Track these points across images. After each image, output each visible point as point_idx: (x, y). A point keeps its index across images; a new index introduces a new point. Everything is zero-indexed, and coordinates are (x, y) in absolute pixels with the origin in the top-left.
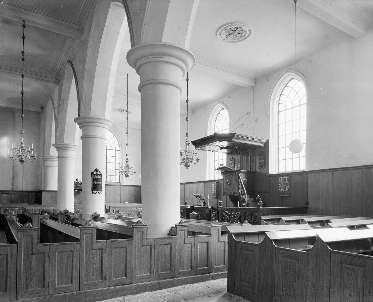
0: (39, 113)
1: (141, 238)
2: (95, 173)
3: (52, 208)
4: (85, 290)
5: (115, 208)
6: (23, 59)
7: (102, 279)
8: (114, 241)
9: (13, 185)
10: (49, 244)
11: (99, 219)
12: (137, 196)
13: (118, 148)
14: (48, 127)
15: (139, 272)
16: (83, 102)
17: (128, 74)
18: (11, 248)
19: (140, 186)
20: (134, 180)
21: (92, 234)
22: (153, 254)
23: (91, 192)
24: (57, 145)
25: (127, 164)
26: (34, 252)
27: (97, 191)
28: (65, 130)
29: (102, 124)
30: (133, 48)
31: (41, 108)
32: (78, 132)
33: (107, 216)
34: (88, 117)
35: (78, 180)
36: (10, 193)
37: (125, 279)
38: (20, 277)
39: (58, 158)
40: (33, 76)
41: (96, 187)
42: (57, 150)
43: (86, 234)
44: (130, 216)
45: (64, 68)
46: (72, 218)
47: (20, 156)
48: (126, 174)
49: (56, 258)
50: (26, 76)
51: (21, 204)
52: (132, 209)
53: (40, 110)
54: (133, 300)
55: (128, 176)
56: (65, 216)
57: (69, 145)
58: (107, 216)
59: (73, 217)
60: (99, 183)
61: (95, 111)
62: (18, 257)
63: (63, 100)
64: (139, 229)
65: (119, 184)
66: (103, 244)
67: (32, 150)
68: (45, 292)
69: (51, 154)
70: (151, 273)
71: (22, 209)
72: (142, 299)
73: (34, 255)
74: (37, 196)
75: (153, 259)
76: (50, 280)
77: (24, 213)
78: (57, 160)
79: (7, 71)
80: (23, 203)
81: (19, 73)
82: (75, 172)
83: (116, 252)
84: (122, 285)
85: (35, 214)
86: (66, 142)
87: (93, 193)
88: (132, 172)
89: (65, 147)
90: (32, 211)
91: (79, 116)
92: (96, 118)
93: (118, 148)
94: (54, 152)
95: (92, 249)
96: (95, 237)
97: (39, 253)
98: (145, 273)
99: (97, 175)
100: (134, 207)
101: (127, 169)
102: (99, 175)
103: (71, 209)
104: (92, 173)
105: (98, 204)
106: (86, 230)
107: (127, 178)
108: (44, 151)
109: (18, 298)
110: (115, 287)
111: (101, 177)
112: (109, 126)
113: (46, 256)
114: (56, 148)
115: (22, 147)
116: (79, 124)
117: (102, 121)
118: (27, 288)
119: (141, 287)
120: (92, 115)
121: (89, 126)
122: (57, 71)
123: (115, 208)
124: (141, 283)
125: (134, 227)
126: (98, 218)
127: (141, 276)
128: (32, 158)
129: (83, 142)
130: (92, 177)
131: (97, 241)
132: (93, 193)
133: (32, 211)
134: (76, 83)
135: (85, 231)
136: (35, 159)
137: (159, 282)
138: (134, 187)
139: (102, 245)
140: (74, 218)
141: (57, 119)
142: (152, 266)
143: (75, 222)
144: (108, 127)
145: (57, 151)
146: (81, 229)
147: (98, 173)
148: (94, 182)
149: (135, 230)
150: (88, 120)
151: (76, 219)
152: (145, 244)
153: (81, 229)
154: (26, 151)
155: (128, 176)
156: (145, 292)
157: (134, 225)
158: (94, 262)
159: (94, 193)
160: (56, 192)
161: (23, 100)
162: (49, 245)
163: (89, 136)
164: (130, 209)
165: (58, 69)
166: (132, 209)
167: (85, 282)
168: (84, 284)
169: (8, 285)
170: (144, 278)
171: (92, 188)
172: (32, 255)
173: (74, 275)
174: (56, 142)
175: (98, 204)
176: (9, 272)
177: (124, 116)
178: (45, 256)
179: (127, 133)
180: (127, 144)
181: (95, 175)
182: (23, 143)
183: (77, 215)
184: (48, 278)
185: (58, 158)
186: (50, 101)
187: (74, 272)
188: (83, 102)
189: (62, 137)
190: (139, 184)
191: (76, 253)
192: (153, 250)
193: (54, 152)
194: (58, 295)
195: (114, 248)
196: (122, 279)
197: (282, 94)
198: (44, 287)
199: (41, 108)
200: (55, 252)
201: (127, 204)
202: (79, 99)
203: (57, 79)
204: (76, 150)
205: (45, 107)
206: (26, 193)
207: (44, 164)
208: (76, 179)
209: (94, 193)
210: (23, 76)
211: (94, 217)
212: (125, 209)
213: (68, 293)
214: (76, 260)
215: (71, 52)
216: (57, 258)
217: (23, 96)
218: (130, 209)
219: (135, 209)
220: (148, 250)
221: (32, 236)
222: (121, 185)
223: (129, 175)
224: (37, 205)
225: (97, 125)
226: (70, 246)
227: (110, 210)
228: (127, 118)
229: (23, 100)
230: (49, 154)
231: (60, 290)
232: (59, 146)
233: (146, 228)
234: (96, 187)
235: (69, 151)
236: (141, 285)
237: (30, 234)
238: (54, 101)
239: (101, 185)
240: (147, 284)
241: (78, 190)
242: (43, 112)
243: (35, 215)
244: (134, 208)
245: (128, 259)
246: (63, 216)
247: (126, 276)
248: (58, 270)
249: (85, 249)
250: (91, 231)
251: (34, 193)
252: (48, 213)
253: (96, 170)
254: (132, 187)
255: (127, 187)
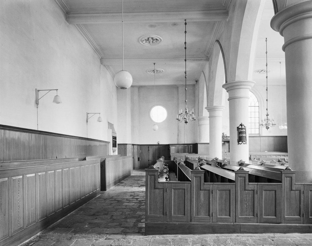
0: (194, 85)
1: (289, 183)
2: (240, 127)
3: (205, 156)
4: (239, 222)
5: (261, 156)
6: (185, 48)
7: (254, 216)
8: (264, 184)
9: (178, 140)
10: (212, 183)
11: (244, 165)
12: (281, 145)
13: (257, 105)
14: (201, 95)
15: (288, 213)
16: (229, 70)
17: (266, 38)
18: (186, 185)
19: (287, 136)
20: (282, 129)
21: (245, 177)
22: (302, 198)
23: (237, 143)
24: (208, 107)
25: (267, 117)
26: (202, 189)
27: (242, 142)
28: (214, 95)
29: (245, 86)
30: (277, 14)
31: (196, 81)
32: (225, 94)
33: (251, 163)
34: (234, 82)
35: (224, 134)
36: (176, 145)
37: (274, 218)
38: (193, 206)
39: (209, 117)
40: (191, 59)
41: (241, 139)
42: (208, 112)
43: (240, 177)
44: (272, 163)
45: (213, 47)
46: (223, 164)
47: (185, 118)
48: (266, 127)
49: (217, 194)
50: (188, 60)
51: (184, 153)
52: (272, 157)
53: (195, 83)
54: (283, 238)
55: (269, 128)
56: (217, 162)
57: (219, 106)
58: (251, 163)
59: (224, 164)
60: (244, 135)
61: (239, 76)
62: (192, 191)
63: (212, 72)
64: (288, 175)
65: (258, 135)
66: (254, 186)
67: (193, 113)
68: (210, 220)
69: (204, 115)
70: (300, 217)
71: (185, 157)
72: (293, 239)
73: (202, 191)
74: (194, 148)
75: (302, 203)
76: (214, 211)
77: (187, 160)
78: (209, 119)
79: (173, 59)
80: (185, 152)
81: (182, 59)
82: (223, 127)
83: (266, 194)
84: (272, 223)
85: (195, 161)
86: (215, 104)
87: (239, 143)
88: (273, 124)
89: (215, 109)
90: (192, 158)
91: (226, 82)
92: (239, 82)
93: (257, 105)
94: (206, 113)
95: (245, 190)
96: (248, 180)
97: (205, 190)
98: (294, 216)
99: (242, 129)
100: (273, 155)
101: (267, 122)
102: (243, 128)
103: (220, 158)
104: (238, 127)
105: (243, 153)
106: (240, 174)
107: (267, 130)
108: (198, 113)
109: (192, 221)
110: (270, 224)
111: (246, 130)
112: (251, 86)
113: (210, 193)
114: (208, 110)
115: (186, 112)
116: (226, 89)
117: (244, 83)
118: (198, 215)
119: (290, 227)
120: (237, 79)
121: (235, 89)
122: (207, 51)
123: (261, 156)
124: (290, 224)
125: (282, 173)
126: (244, 164)
127: (290, 218)
128: (193, 119)
129: (229, 103)
130: (238, 130)
131: (249, 183)
132: (239, 143)
133: (192, 158)
134: (223, 56)
135: (240, 175)
136: (195, 120)
137: (309, 226)
138: (273, 138)
139: (253, 187)
140: (224, 164)
141: (208, 88)
142: (301, 210)
143: (225, 167)
144: (250, 87)
145: (209, 113)
146: (236, 173)
147: (243, 127)
148: (239, 134)
149: (283, 175)
150: (234, 84)
151: (226, 165)
152: (294, 189)
153: (236, 173)
154: (189, 114)
155: (269, 128)
156: (295, 232)
157: (283, 171)
158: (247, 201)
159: (240, 144)
160: (208, 144)
161: (186, 78)
162: (213, 184)
163: (235, 98)
164: (270, 157)
165: (208, 48)
166: (272, 157)
167: (240, 216)
168: (239, 218)
169: (186, 210)
170: (293, 220)
171: (238, 139)
172: (201, 191)
173: (231, 209)
174: (207, 106)
175: (243, 153)
176: (186, 202)
177: (264, 75)
178: (209, 192)
179: (267, 90)
180: (267, 100)
181: (240, 129)
182: (187, 109)
183: (227, 162)
184: (212, 210)
185: (209, 117)
186: (202, 75)
187: (231, 207)
188: (229, 70)
189: (212, 101)
190: (285, 134)
191: (233, 192)
192: (302, 195)
193: (206, 113)
194: (219, 223)
195: (264, 190)
196: (272, 218)
197: (39, 99)
198: (209, 215)
199: (196, 81)
200: (217, 190)
201: (267, 153)
202: (226, 68)
203: (208, 57)
204: (222, 110)
205: (198, 80)
206: (186, 145)
207: (199, 123)
208: (223, 133)
209: (240, 144)
210: (185, 61)
211: (240, 163)
212: (265, 157)
213: (227, 223)
214: (233, 197)
215: (219, 33)
216: (218, 195)
217: (186, 75)
218: (270, 157)
219: (275, 157)
220: (297, 195)
221: (200, 177)
222: (260, 137)
223: (269, 127)
224: (194, 154)
225: (241, 87)
226: (227, 186)
227: (251, 158)
228: (267, 77)
229: (186, 78)
230: (202, 115)
231: (221, 220)
232: (210, 108)
233: (294, 174)
234: (241, 139)
235: (217, 111)
236: (291, 226)
237: (199, 175)
238: (205, 74)
239: (246, 137)
240: (296, 226)
241: (224, 141)
242: (197, 84)
243: (195, 162)
244: (274, 156)
245: (277, 202)
246: (215, 163)
247: (275, 216)
248: (219, 204)
249: (240, 189)
250: (244, 175)
251: (192, 145)
252: (205, 160)
253: (241, 125)
254: (267, 138)
255: (267, 138)
